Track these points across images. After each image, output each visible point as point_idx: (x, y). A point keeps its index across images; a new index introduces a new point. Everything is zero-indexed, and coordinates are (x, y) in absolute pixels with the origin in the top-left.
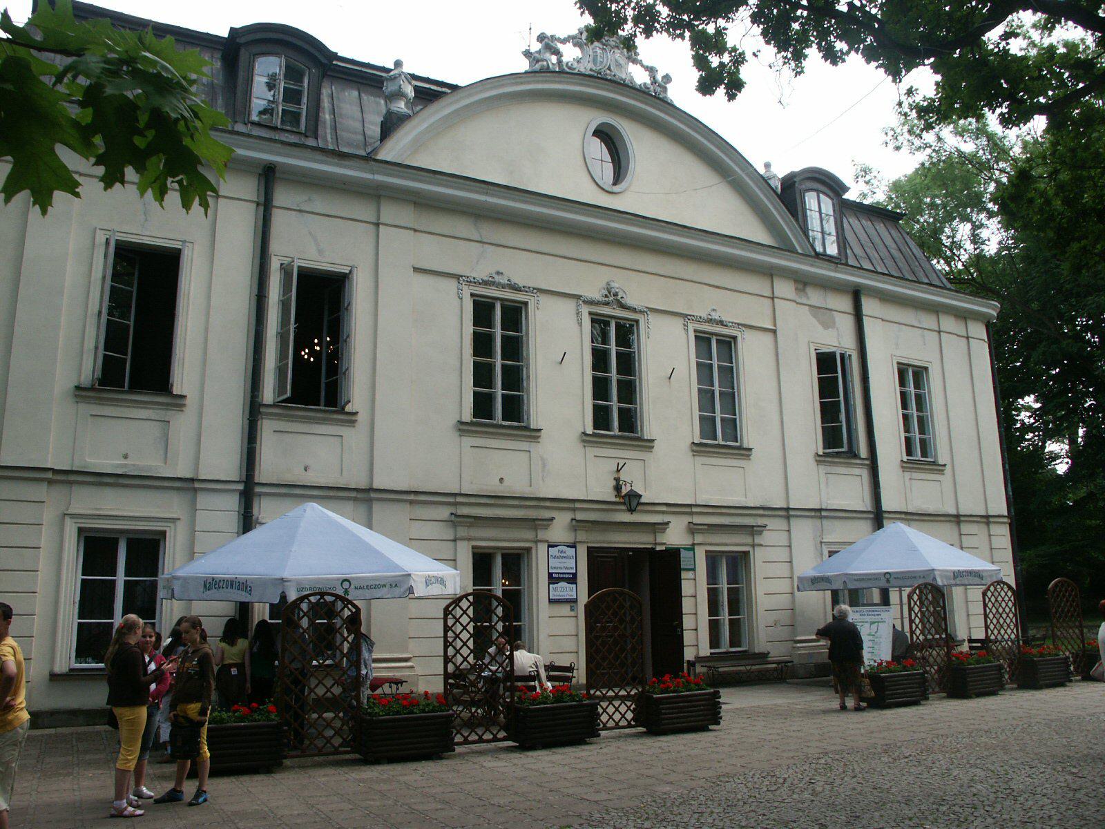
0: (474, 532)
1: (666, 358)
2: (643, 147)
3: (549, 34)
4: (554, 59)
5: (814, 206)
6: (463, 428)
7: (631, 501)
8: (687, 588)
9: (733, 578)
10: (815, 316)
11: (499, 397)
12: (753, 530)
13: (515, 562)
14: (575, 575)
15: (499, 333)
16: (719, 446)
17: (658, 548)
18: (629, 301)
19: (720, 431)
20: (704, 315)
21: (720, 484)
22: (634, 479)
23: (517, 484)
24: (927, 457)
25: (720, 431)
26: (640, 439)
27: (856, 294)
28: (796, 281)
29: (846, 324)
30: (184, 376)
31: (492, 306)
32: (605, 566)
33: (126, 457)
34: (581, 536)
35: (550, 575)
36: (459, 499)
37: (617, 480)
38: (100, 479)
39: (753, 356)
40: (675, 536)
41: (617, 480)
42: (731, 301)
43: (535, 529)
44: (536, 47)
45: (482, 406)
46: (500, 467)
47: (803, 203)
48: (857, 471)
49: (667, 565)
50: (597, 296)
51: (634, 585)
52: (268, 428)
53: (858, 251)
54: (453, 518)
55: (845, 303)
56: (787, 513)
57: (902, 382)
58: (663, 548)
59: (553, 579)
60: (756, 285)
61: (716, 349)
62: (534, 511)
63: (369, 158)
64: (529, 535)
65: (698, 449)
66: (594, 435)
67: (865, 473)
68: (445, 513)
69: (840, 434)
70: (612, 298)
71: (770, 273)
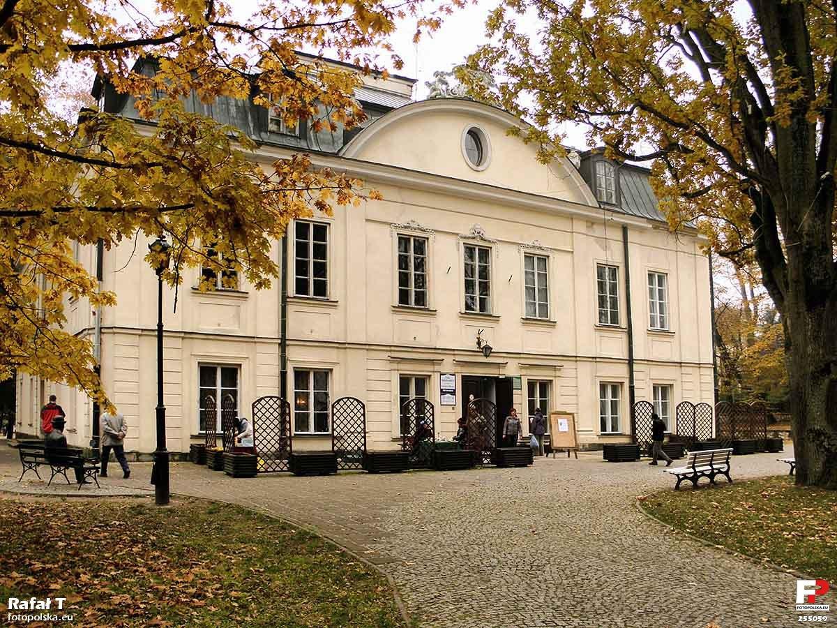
0: (402, 366)
1: (507, 270)
2: (497, 143)
3: (440, 71)
4: (444, 87)
5: (602, 172)
6: (395, 310)
7: (487, 351)
8: (516, 399)
9: (543, 394)
10: (597, 243)
11: (412, 293)
12: (554, 367)
13: (421, 382)
14: (455, 390)
15: (412, 253)
16: (609, 326)
17: (501, 377)
18: (486, 236)
19: (539, 312)
20: (531, 244)
21: (537, 342)
22: (488, 340)
23: (423, 341)
24: (617, 430)
25: (539, 312)
26: (328, 300)
27: (625, 229)
28: (587, 221)
29: (617, 247)
30: (433, 300)
31: (409, 239)
32: (470, 384)
33: (219, 325)
34: (459, 369)
35: (441, 390)
36: (393, 348)
37: (479, 339)
38: (207, 336)
39: (558, 269)
40: (511, 370)
41: (479, 339)
42: (545, 236)
43: (434, 364)
44: (433, 79)
45: (404, 297)
46: (415, 330)
47: (595, 170)
48: (619, 335)
49: (505, 386)
50: (468, 234)
51: (487, 393)
52: (291, 309)
53: (630, 200)
54: (389, 358)
55: (618, 235)
56: (576, 358)
57: (651, 283)
58: (504, 377)
59: (443, 392)
60: (563, 224)
61: (537, 262)
62: (433, 356)
63: (335, 155)
64: (430, 368)
65: (600, 328)
66: (466, 313)
67: (625, 337)
68: (385, 355)
69: (610, 310)
70: (476, 234)
71: (571, 217)
